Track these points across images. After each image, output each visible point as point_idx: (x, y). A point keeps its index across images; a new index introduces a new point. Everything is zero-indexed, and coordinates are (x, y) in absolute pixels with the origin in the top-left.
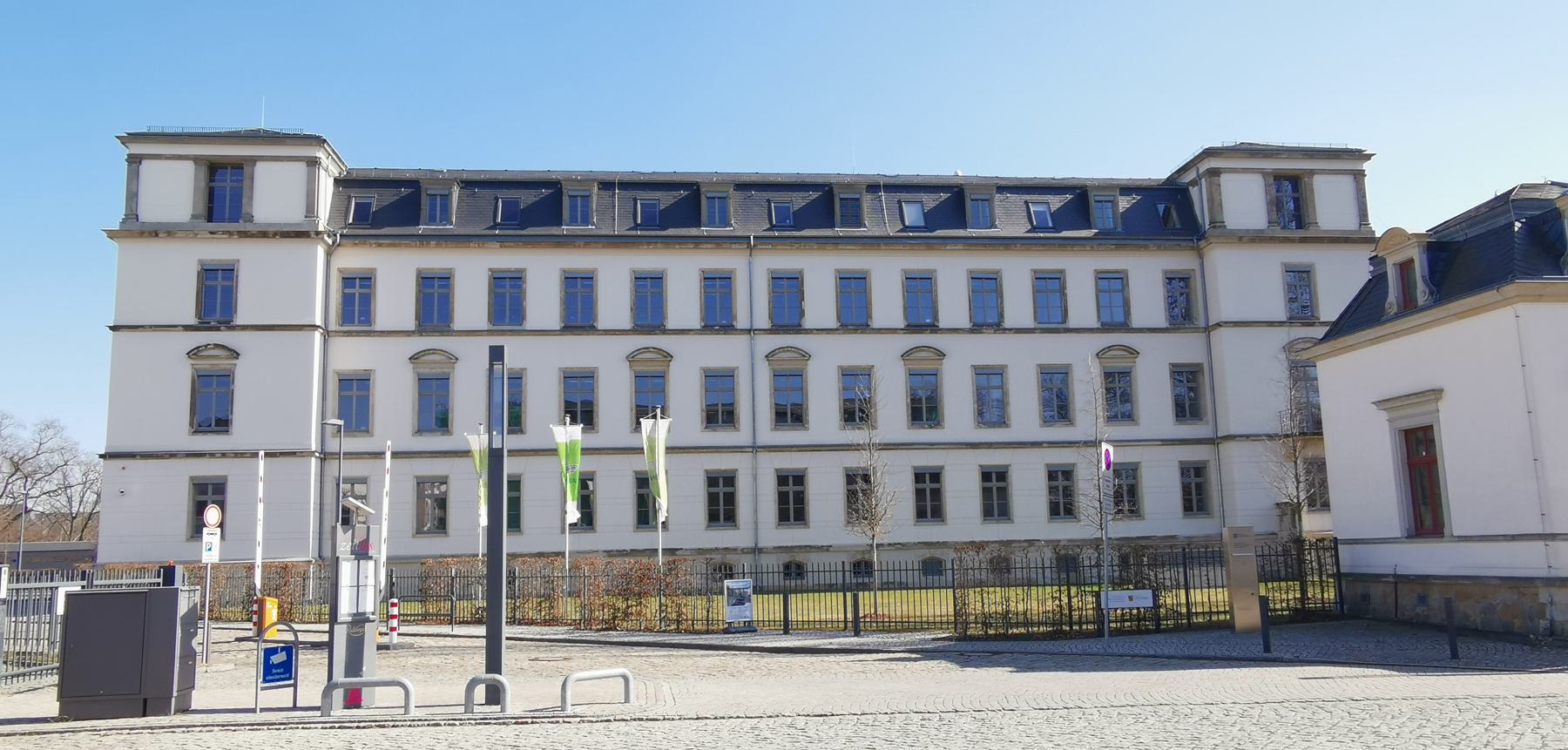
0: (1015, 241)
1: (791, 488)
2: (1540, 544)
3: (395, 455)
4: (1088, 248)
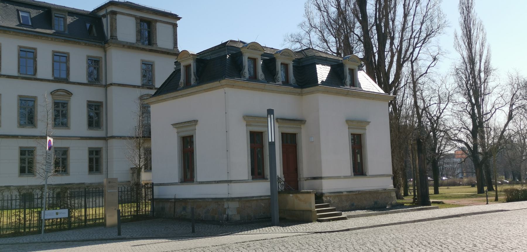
0: (9, 30)
2: (226, 185)
4: (50, 39)
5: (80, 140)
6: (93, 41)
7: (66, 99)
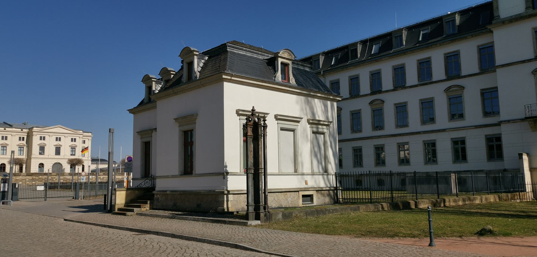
4: (439, 45)
5: (475, 129)
6: (479, 30)
7: (454, 94)
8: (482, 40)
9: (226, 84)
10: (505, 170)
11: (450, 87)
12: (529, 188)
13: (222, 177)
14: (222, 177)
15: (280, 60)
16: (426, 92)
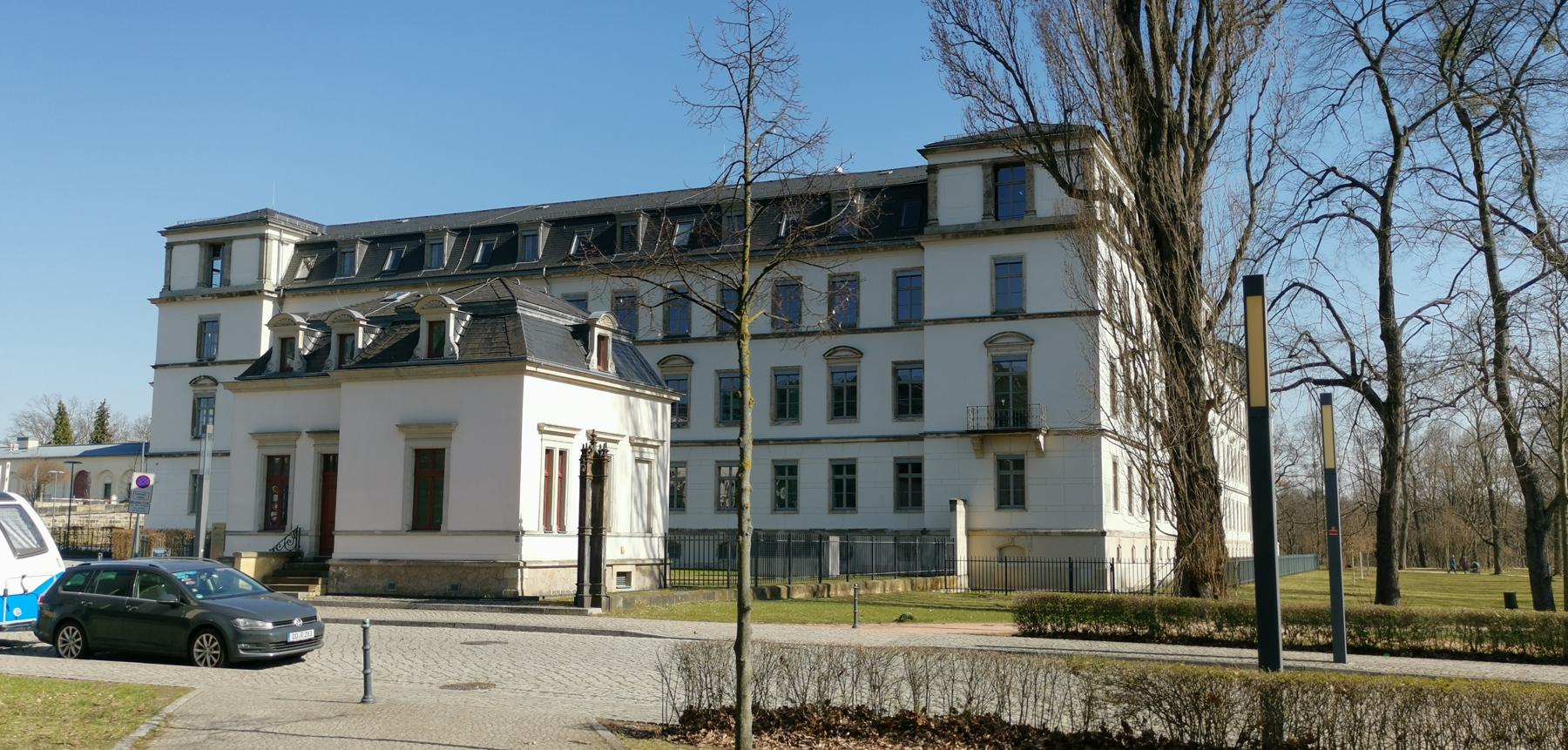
1: (845, 476)
3: (214, 454)
8: (902, 260)
9: (527, 380)
10: (924, 532)
11: (835, 350)
12: (962, 568)
13: (513, 538)
14: (513, 538)
15: (597, 331)
16: (785, 353)
